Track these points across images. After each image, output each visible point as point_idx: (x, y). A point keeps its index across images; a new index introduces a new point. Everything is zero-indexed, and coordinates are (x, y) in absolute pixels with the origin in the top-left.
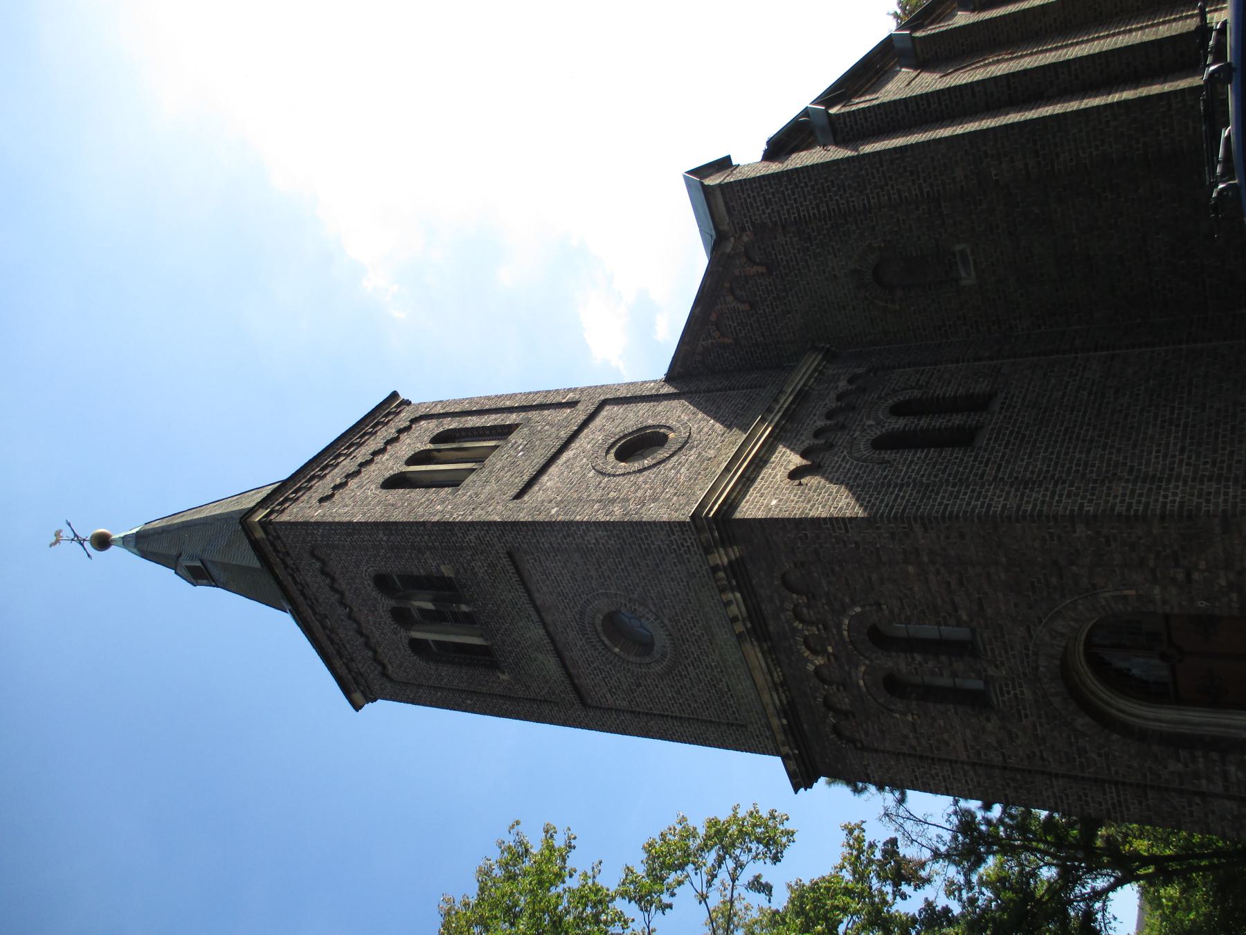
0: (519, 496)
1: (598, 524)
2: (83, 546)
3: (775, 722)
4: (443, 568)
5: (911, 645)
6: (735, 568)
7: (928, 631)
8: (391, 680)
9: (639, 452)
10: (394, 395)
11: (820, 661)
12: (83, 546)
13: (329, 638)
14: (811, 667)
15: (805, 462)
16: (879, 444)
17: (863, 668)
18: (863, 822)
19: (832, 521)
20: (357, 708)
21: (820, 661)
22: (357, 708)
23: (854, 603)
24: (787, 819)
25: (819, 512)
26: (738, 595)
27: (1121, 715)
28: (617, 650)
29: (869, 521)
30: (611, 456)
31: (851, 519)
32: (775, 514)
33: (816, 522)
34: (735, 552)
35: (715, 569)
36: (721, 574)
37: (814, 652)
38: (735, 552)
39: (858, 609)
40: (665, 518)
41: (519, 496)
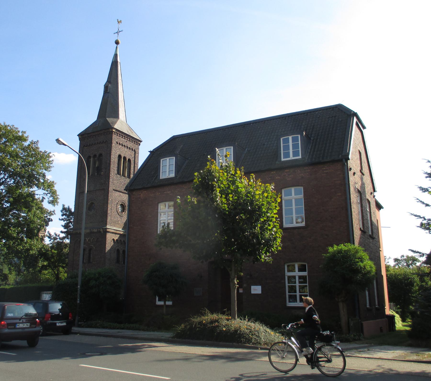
0: (114, 190)
1: (107, 209)
2: (116, 33)
3: (78, 231)
4: (103, 172)
5: (90, 254)
6: (100, 232)
7: (91, 256)
8: (83, 147)
9: (122, 206)
10: (141, 141)
11: (87, 240)
12: (116, 33)
13: (91, 136)
14: (86, 239)
15: (115, 240)
16: (118, 250)
17: (86, 247)
18: (56, 214)
19: (105, 248)
20: (78, 135)
21: (87, 240)
22: (78, 135)
23: (95, 247)
24: (57, 205)
25: (107, 245)
26: (96, 231)
27: (88, 332)
28: (89, 204)
29: (105, 253)
30: (121, 203)
31: (105, 250)
32: (107, 239)
33: (105, 245)
34: (102, 232)
35: (100, 229)
36: (99, 230)
37: (89, 240)
38: (102, 232)
39: (94, 248)
40: (108, 221)
41: (114, 190)
